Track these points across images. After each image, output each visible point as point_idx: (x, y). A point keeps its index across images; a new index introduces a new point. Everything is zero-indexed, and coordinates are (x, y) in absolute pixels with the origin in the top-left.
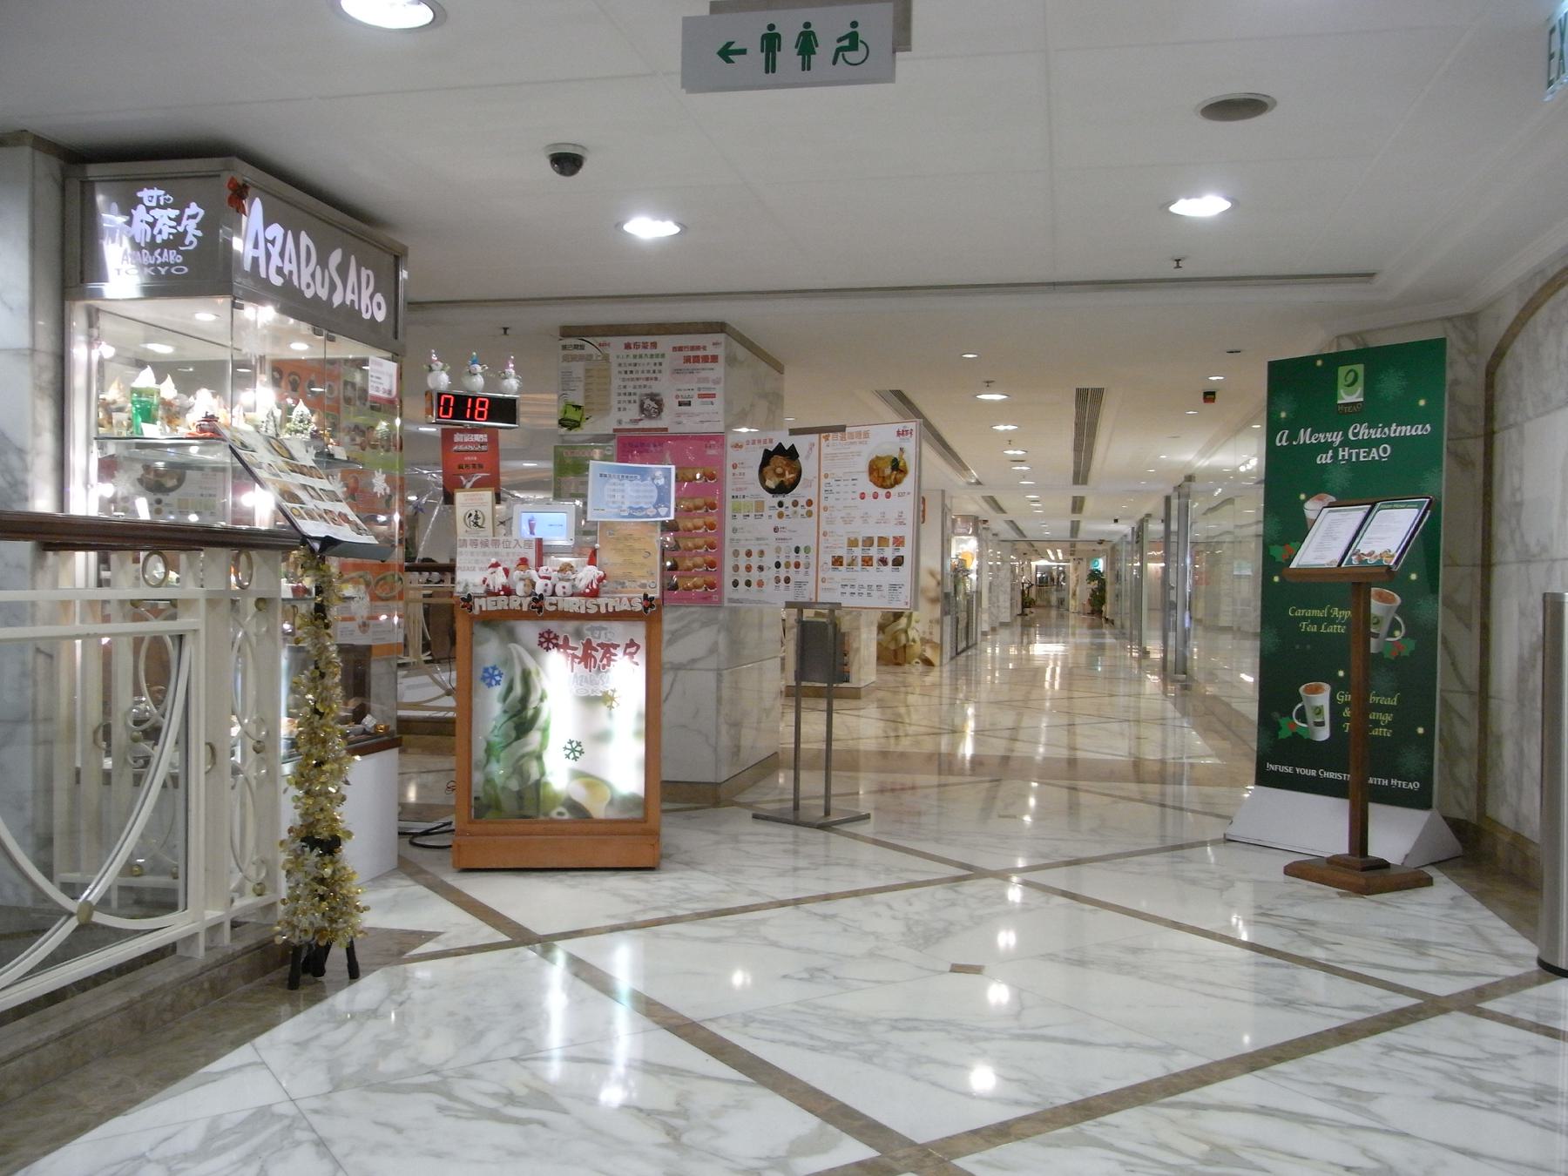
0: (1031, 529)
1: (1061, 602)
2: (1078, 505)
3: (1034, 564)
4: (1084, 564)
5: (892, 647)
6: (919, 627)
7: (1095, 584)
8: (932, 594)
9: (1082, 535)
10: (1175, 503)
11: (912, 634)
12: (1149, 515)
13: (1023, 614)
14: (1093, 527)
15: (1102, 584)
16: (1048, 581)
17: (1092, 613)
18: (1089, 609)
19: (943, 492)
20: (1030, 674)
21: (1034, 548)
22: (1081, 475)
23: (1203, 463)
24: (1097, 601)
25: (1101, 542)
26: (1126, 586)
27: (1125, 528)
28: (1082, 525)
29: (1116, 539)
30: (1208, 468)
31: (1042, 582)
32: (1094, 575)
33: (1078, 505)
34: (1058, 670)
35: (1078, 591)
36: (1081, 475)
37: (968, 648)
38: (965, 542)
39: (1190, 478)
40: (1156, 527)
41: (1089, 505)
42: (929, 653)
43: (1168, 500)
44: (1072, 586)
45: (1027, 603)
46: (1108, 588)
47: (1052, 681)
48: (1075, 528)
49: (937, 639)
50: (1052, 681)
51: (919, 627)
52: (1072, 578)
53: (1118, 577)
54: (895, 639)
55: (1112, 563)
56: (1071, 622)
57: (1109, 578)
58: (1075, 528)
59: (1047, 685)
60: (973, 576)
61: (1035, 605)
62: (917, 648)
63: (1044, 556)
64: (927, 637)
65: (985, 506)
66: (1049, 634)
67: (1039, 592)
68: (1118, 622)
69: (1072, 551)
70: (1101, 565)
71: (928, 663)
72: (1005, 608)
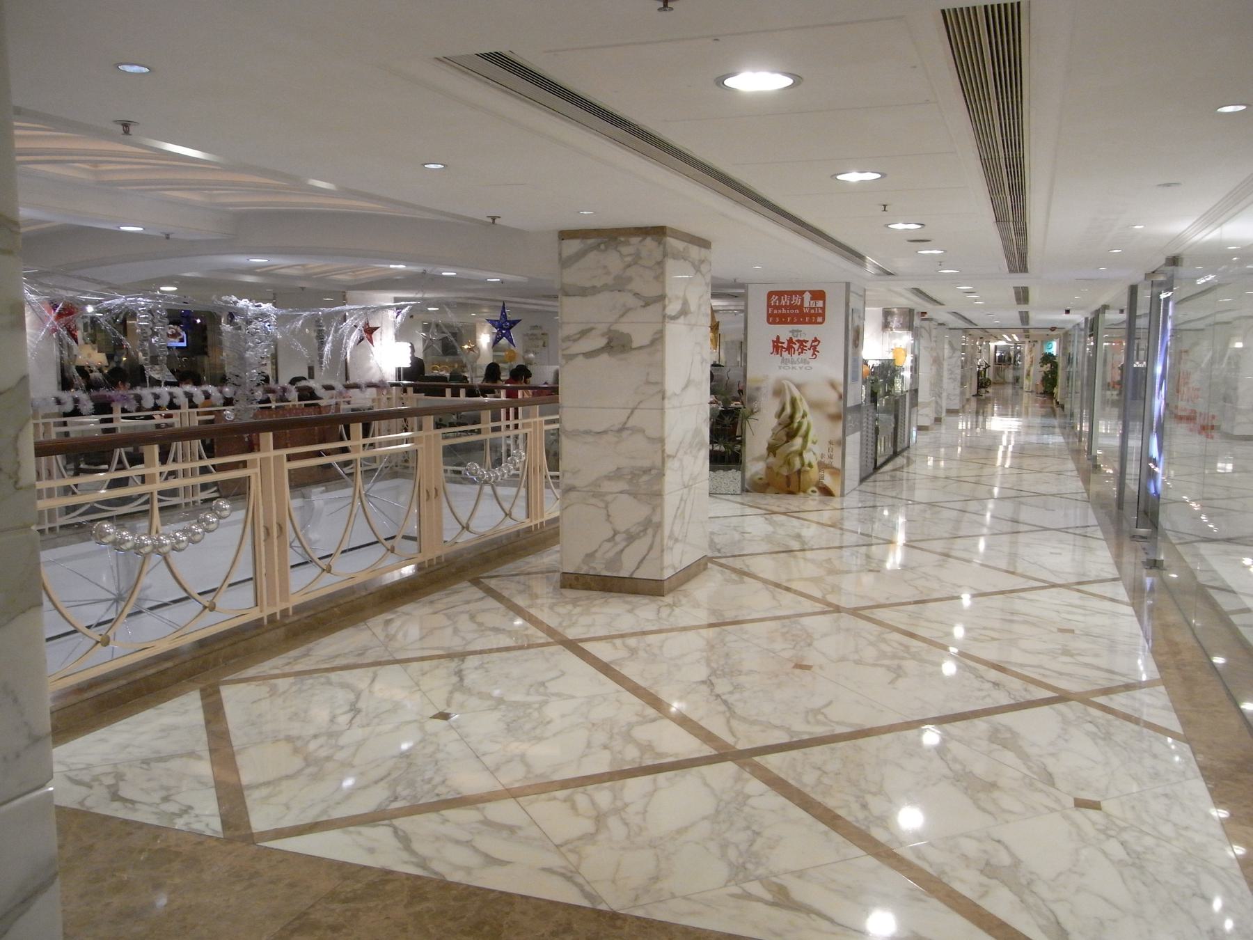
0: (981, 318)
1: (1017, 380)
2: (1022, 296)
3: (992, 345)
4: (1038, 345)
5: (784, 471)
6: (816, 448)
7: (1047, 367)
8: (833, 410)
9: (1032, 323)
10: (1144, 296)
11: (808, 457)
12: (1105, 307)
13: (978, 395)
14: (1040, 317)
15: (1055, 366)
16: (1005, 360)
17: (1045, 393)
18: (1041, 389)
19: (848, 285)
20: (984, 449)
21: (987, 333)
22: (1018, 261)
23: (1211, 235)
24: (1049, 382)
25: (1053, 329)
26: (1080, 366)
27: (1078, 317)
28: (1032, 315)
29: (1069, 326)
30: (1209, 244)
31: (1001, 360)
32: (1048, 358)
33: (1022, 296)
34: (1010, 448)
35: (1032, 373)
36: (1018, 261)
37: (896, 454)
38: (900, 336)
39: (1174, 261)
40: (1114, 316)
41: (1034, 295)
42: (828, 481)
43: (1133, 290)
44: (1026, 366)
45: (983, 384)
46: (1060, 372)
47: (1003, 459)
48: (1024, 317)
49: (837, 463)
50: (1003, 459)
51: (816, 448)
52: (1027, 359)
53: (1069, 361)
54: (788, 462)
55: (1064, 347)
56: (1025, 400)
57: (1061, 362)
58: (1024, 317)
59: (999, 462)
60: (907, 374)
61: (988, 385)
62: (814, 474)
63: (997, 339)
64: (827, 461)
65: (916, 299)
66: (1009, 408)
67: (997, 371)
68: (1067, 406)
69: (1026, 333)
70: (1054, 348)
71: (826, 492)
72: (952, 391)
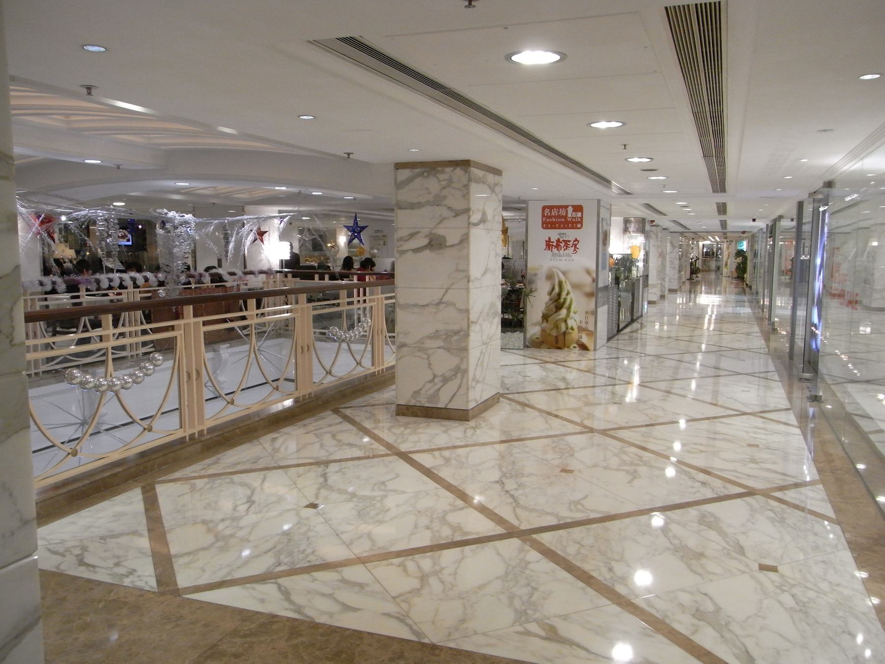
0: (693, 225)
1: (718, 268)
2: (722, 209)
3: (701, 244)
4: (733, 244)
5: (554, 333)
6: (576, 317)
7: (740, 260)
8: (588, 289)
9: (729, 228)
10: (808, 209)
11: (571, 323)
12: (781, 217)
13: (691, 279)
14: (734, 224)
15: (745, 259)
16: (710, 254)
17: (738, 277)
18: (735, 275)
19: (599, 201)
20: (695, 317)
21: (697, 235)
22: (719, 184)
23: (855, 166)
24: (741, 270)
25: (744, 232)
26: (763, 259)
27: (761, 224)
28: (729, 222)
29: (755, 231)
30: (854, 173)
31: (707, 254)
32: (740, 253)
33: (722, 209)
34: (714, 317)
35: (729, 263)
36: (719, 184)
37: (633, 321)
38: (636, 237)
39: (829, 184)
40: (787, 223)
41: (730, 209)
42: (585, 340)
43: (800, 205)
44: (725, 259)
45: (694, 271)
46: (749, 263)
47: (708, 324)
48: (724, 224)
49: (591, 327)
50: (708, 324)
51: (576, 317)
52: (726, 253)
53: (755, 255)
54: (557, 327)
55: (751, 245)
56: (724, 283)
57: (749, 256)
58: (724, 224)
59: (706, 327)
60: (640, 264)
61: (697, 272)
62: (575, 335)
63: (704, 239)
64: (584, 325)
65: (647, 211)
66: (712, 288)
67: (704, 262)
68: (754, 287)
69: (725, 235)
70: (744, 246)
71: (584, 347)
72: (672, 276)
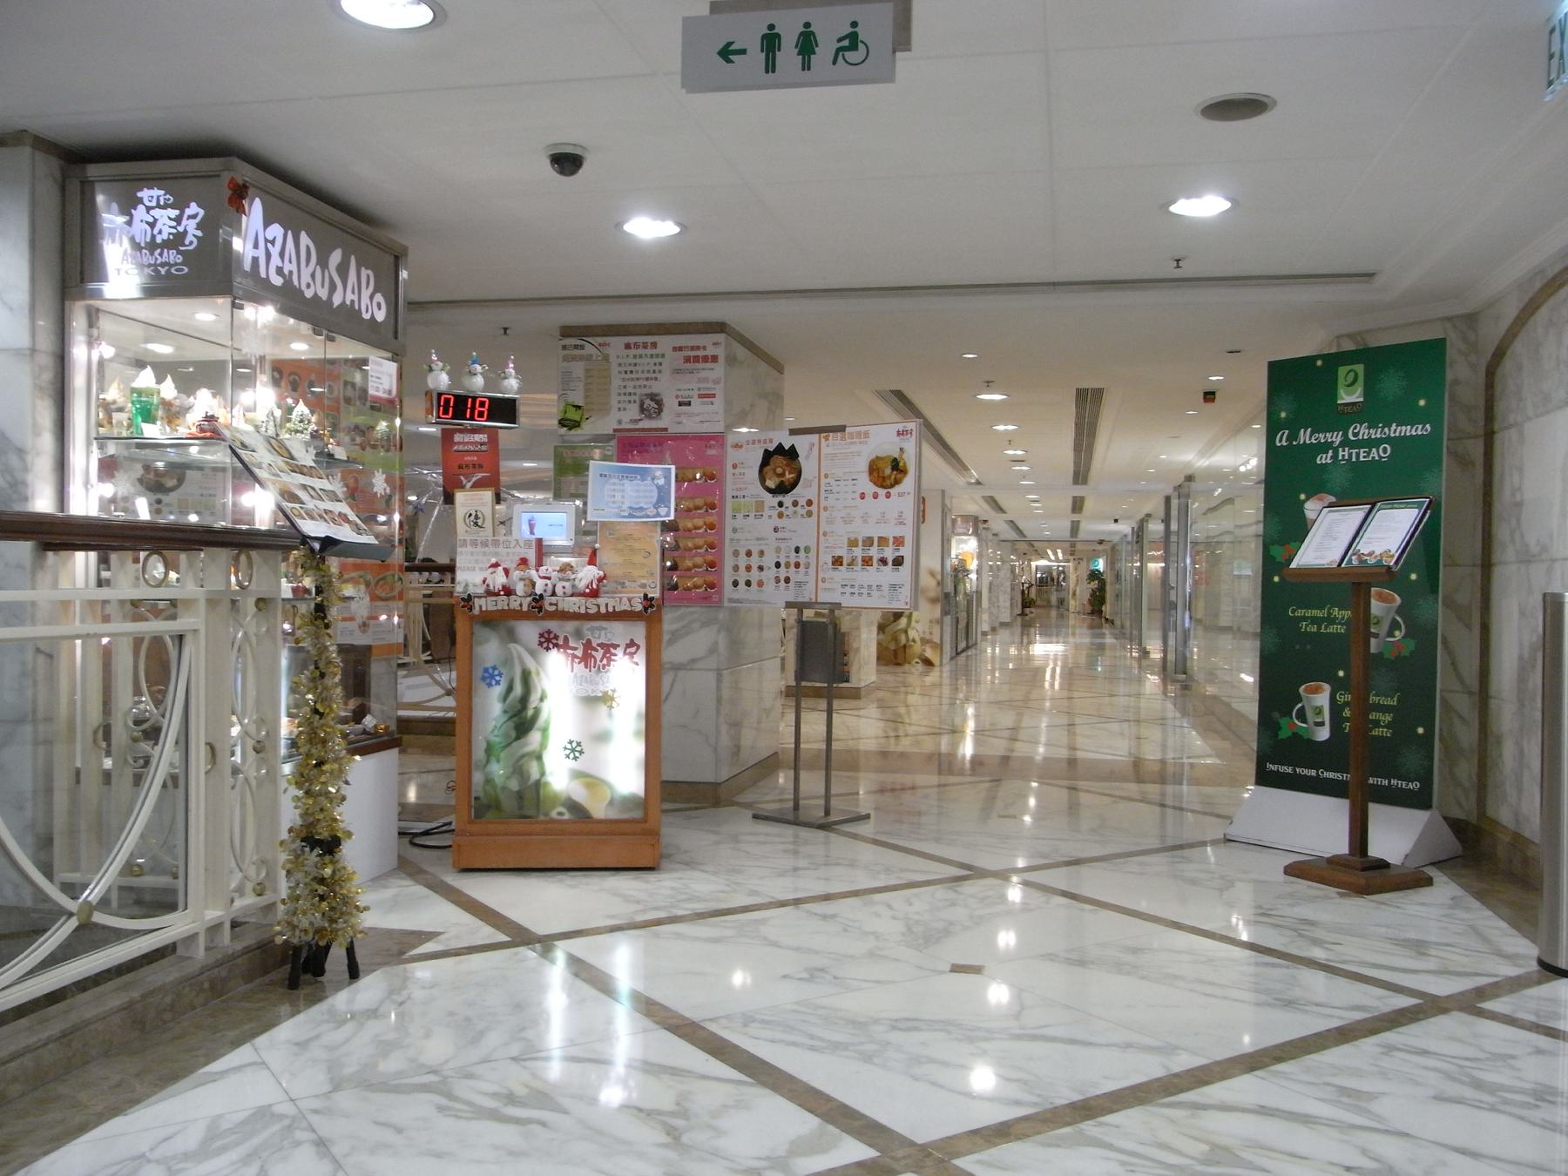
0: (1031, 529)
1: (1061, 602)
2: (1078, 505)
3: (1034, 564)
4: (1084, 564)
5: (892, 647)
6: (919, 627)
7: (1095, 584)
8: (932, 594)
9: (1082, 535)
10: (1175, 503)
11: (912, 634)
12: (1149, 515)
13: (1023, 614)
14: (1093, 527)
15: (1102, 584)
16: (1048, 581)
17: (1092, 613)
18: (1089, 609)
19: (943, 492)
20: (1030, 674)
21: (1034, 548)
22: (1081, 475)
23: (1203, 463)
24: (1097, 601)
25: (1101, 542)
26: (1126, 586)
27: (1125, 528)
28: (1082, 525)
29: (1116, 539)
30: (1208, 468)
31: (1042, 582)
32: (1094, 575)
33: (1078, 505)
34: (1058, 670)
35: (1078, 591)
36: (1081, 475)
37: (968, 648)
38: (965, 542)
39: (1190, 478)
40: (1156, 527)
41: (1089, 505)
42: (929, 653)
43: (1168, 500)
44: (1072, 586)
45: (1027, 603)
46: (1108, 588)
47: (1052, 681)
48: (1075, 528)
49: (937, 639)
50: (1052, 681)
51: (919, 627)
52: (1072, 578)
53: (1118, 577)
54: (895, 639)
55: (1112, 563)
56: (1071, 622)
57: (1109, 578)
58: (1075, 528)
59: (1047, 685)
60: (973, 576)
61: (1035, 605)
62: (917, 648)
63: (1044, 556)
64: (927, 637)
65: (985, 506)
66: (1049, 634)
67: (1039, 592)
68: (1118, 622)
69: (1072, 551)
70: (1101, 565)
71: (928, 663)
72: (1005, 608)
